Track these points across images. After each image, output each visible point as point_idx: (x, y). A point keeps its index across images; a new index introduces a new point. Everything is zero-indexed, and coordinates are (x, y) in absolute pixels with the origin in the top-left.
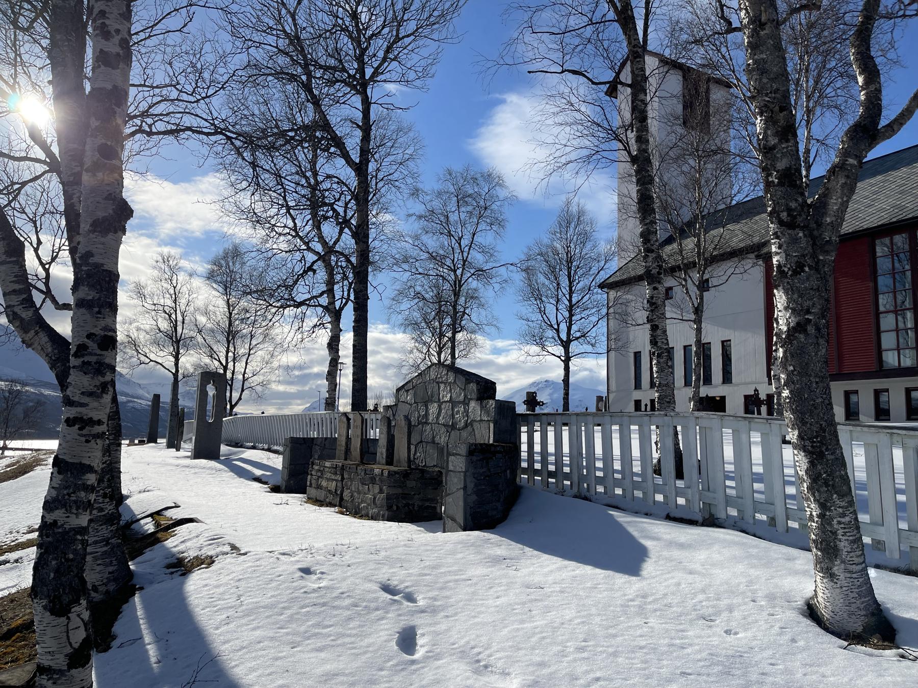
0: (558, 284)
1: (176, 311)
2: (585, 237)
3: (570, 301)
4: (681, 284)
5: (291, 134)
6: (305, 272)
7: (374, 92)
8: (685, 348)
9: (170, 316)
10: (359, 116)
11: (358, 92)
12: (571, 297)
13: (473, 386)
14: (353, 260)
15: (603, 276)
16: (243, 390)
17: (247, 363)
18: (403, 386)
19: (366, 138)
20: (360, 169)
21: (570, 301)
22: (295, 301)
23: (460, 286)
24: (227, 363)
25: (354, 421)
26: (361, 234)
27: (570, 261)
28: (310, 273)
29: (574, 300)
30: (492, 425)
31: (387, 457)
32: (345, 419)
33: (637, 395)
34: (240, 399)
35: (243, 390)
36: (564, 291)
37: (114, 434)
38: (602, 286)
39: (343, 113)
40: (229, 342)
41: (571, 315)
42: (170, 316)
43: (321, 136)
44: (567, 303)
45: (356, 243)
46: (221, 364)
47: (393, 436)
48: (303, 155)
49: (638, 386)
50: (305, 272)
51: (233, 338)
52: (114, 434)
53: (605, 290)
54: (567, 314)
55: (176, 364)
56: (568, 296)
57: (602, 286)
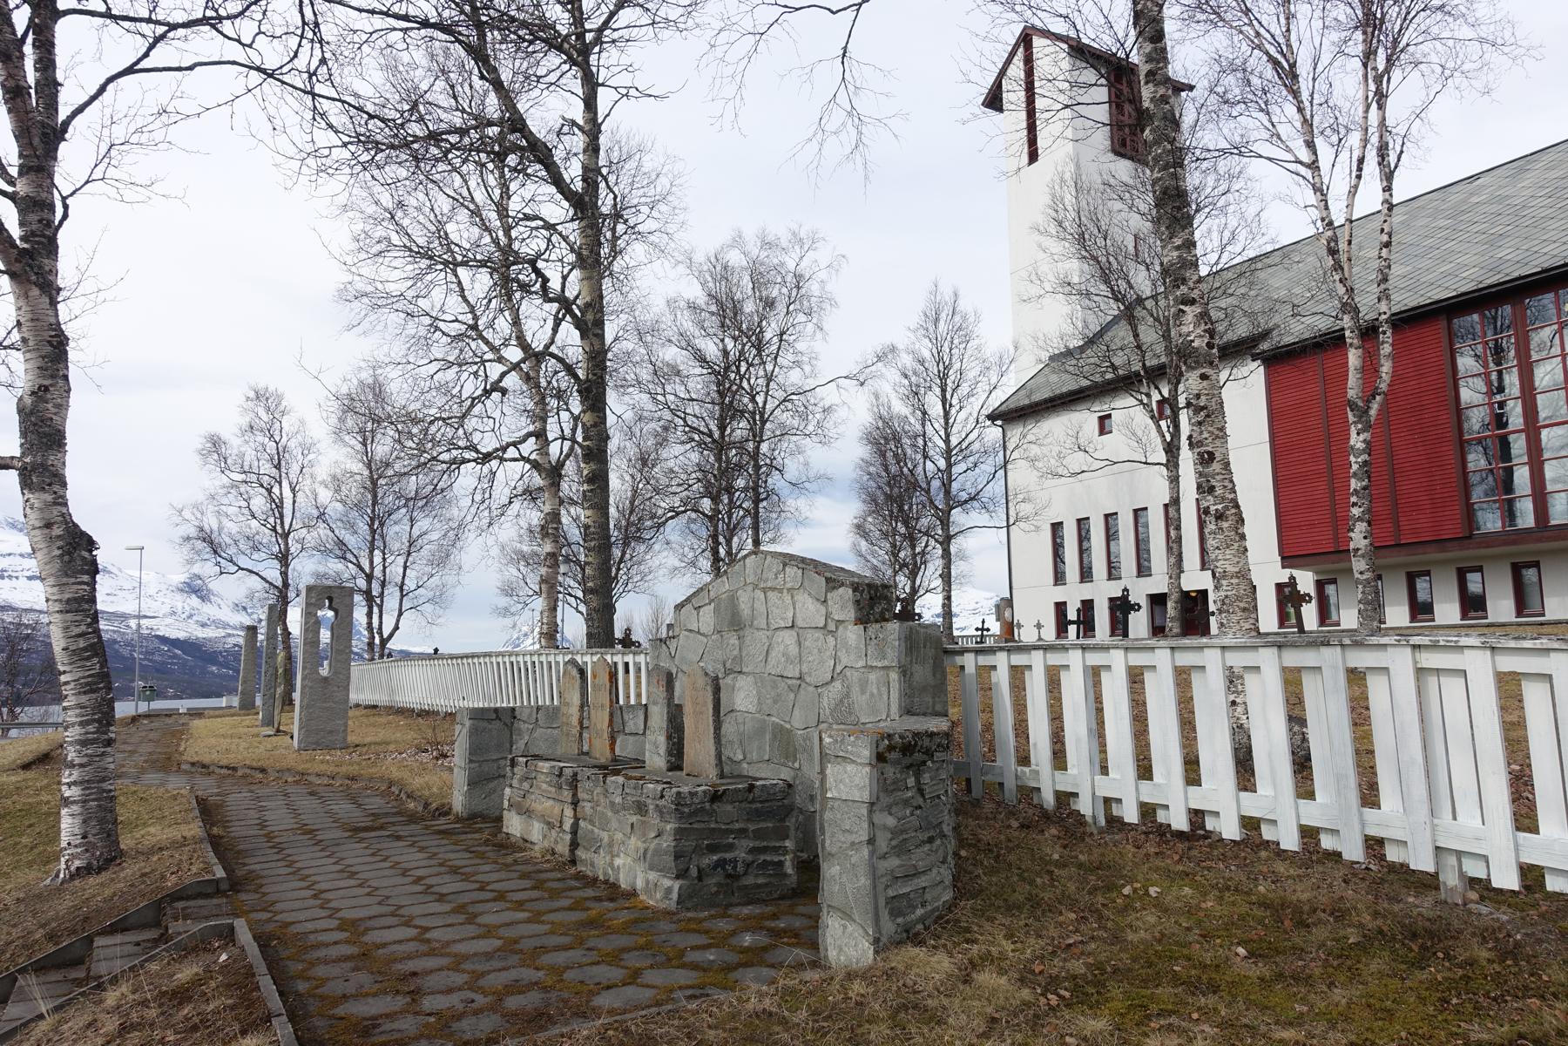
0: (924, 413)
1: (280, 483)
2: (963, 333)
3: (947, 441)
4: (1141, 401)
5: (454, 139)
6: (487, 393)
7: (605, 62)
8: (1138, 513)
9: (269, 491)
10: (577, 112)
11: (574, 63)
12: (948, 435)
13: (846, 593)
14: (581, 374)
15: (995, 401)
16: (400, 614)
17: (405, 568)
18: (688, 600)
19: (593, 148)
20: (583, 204)
21: (947, 441)
22: (477, 451)
23: (764, 422)
24: (372, 567)
25: (594, 676)
26: (591, 323)
27: (943, 377)
28: (496, 396)
29: (954, 441)
30: (894, 676)
31: (669, 753)
32: (575, 672)
33: (1059, 594)
34: (396, 628)
35: (400, 614)
36: (936, 425)
37: (99, 721)
38: (992, 417)
39: (550, 108)
40: (373, 532)
41: (950, 465)
42: (269, 491)
43: (514, 144)
44: (942, 445)
45: (582, 338)
46: (362, 569)
47: (679, 707)
48: (480, 185)
49: (1059, 578)
50: (487, 393)
51: (382, 524)
52: (99, 721)
53: (999, 422)
54: (942, 463)
55: (284, 574)
56: (942, 433)
57: (992, 417)
